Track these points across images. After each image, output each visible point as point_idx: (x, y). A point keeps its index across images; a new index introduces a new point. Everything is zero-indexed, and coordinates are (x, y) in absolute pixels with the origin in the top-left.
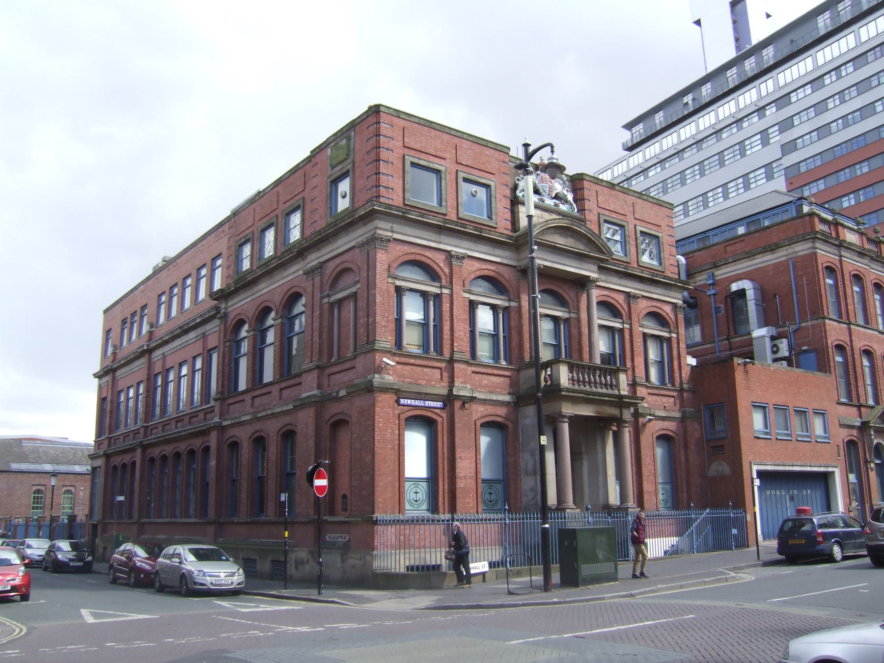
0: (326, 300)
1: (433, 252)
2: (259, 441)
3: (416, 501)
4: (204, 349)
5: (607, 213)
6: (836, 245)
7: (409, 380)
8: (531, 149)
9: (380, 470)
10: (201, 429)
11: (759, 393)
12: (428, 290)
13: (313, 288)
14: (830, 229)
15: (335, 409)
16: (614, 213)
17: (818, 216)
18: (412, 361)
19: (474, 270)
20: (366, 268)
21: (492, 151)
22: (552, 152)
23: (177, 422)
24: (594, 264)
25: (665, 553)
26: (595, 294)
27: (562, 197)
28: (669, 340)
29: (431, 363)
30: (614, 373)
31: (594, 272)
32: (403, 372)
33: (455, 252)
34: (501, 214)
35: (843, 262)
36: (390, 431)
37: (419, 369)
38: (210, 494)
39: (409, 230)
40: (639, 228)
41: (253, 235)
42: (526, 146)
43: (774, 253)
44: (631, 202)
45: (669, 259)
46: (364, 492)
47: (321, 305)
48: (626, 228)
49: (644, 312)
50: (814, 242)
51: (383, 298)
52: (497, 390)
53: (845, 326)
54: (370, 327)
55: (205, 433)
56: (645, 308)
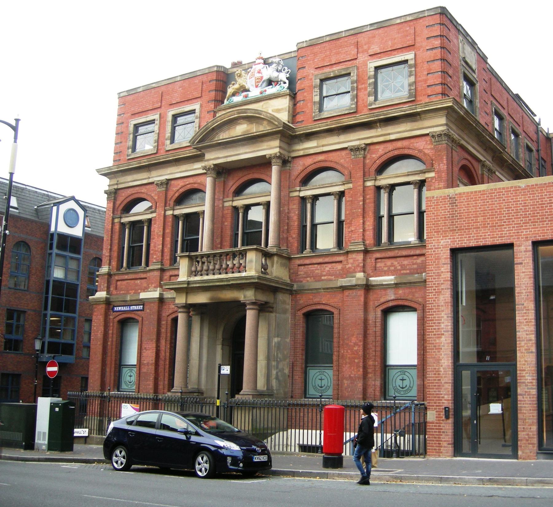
3: (403, 388)
7: (123, 292)
32: (122, 287)
36: (100, 332)
37: (132, 281)
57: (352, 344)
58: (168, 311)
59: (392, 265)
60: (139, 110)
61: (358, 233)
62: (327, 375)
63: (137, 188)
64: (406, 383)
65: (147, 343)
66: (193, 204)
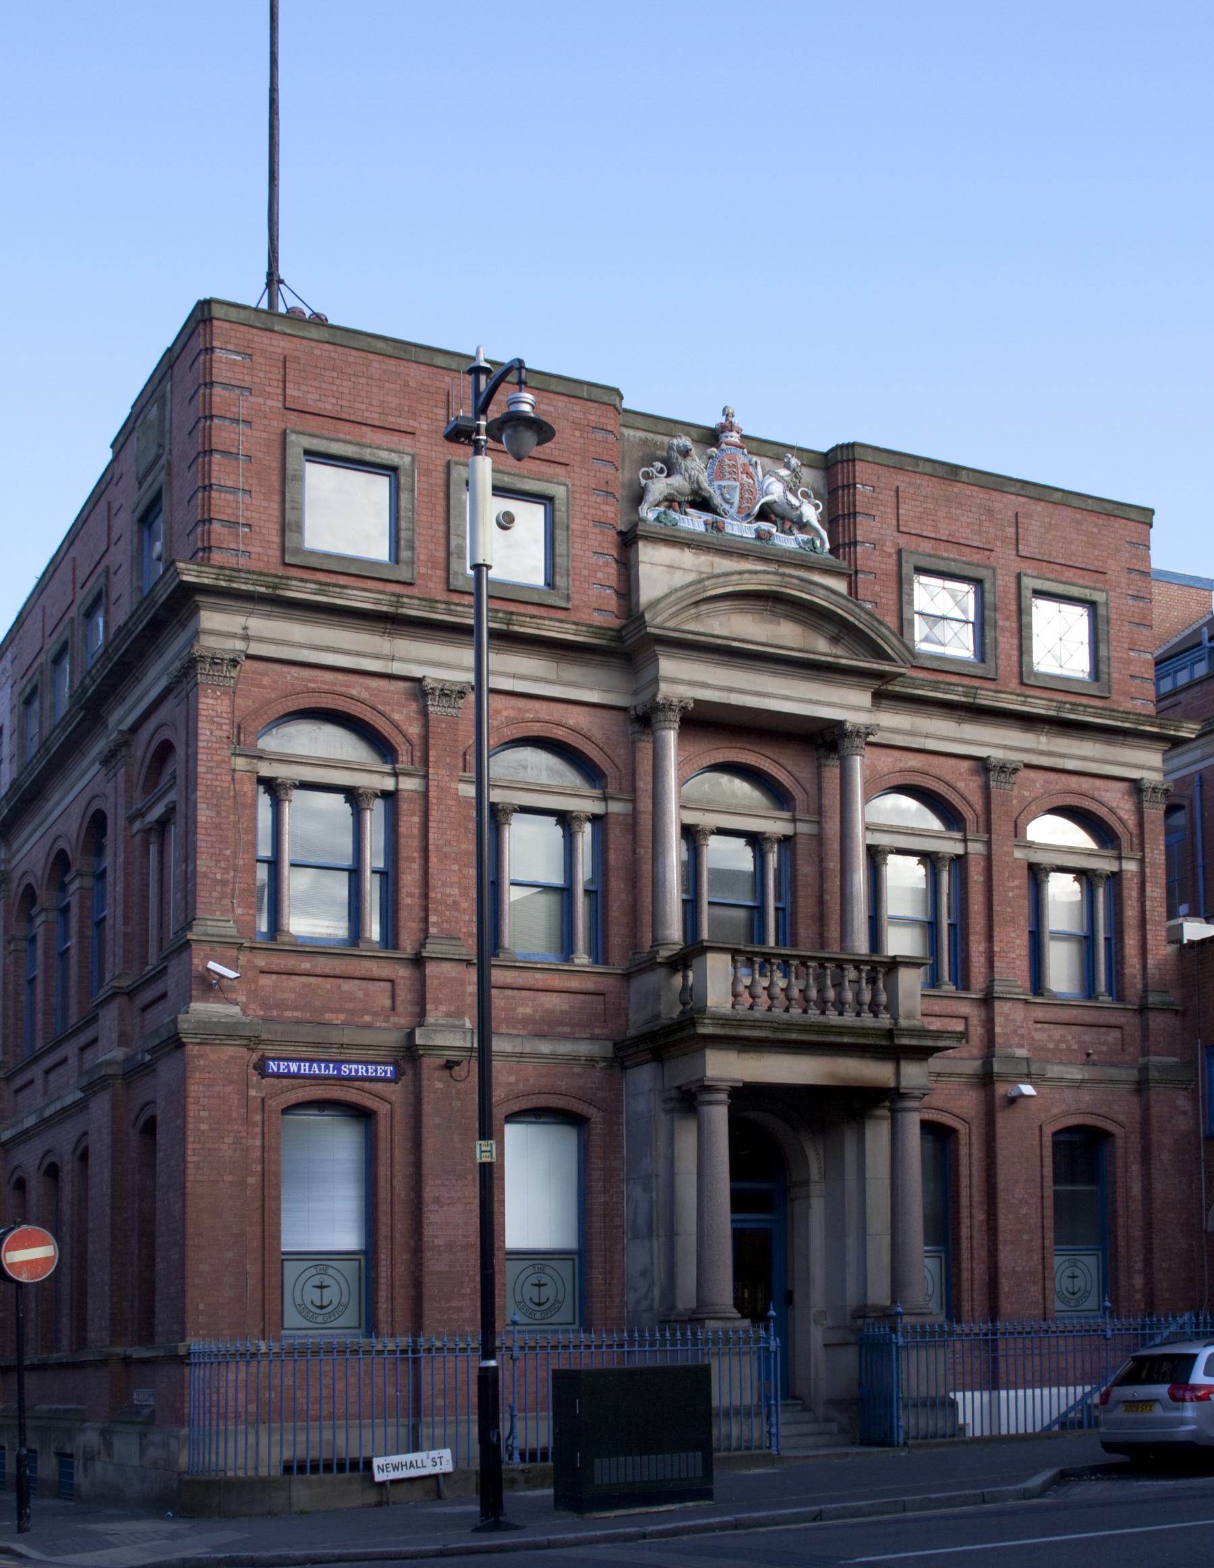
0: (137, 826)
2: (52, 1172)
5: (926, 546)
12: (357, 784)
33: (436, 680)
36: (229, 1140)
37: (328, 984)
41: (42, 673)
52: (560, 1029)
57: (1015, 1201)
60: (320, 404)
61: (1007, 960)
62: (1083, 1267)
63: (329, 676)
65: (443, 1185)
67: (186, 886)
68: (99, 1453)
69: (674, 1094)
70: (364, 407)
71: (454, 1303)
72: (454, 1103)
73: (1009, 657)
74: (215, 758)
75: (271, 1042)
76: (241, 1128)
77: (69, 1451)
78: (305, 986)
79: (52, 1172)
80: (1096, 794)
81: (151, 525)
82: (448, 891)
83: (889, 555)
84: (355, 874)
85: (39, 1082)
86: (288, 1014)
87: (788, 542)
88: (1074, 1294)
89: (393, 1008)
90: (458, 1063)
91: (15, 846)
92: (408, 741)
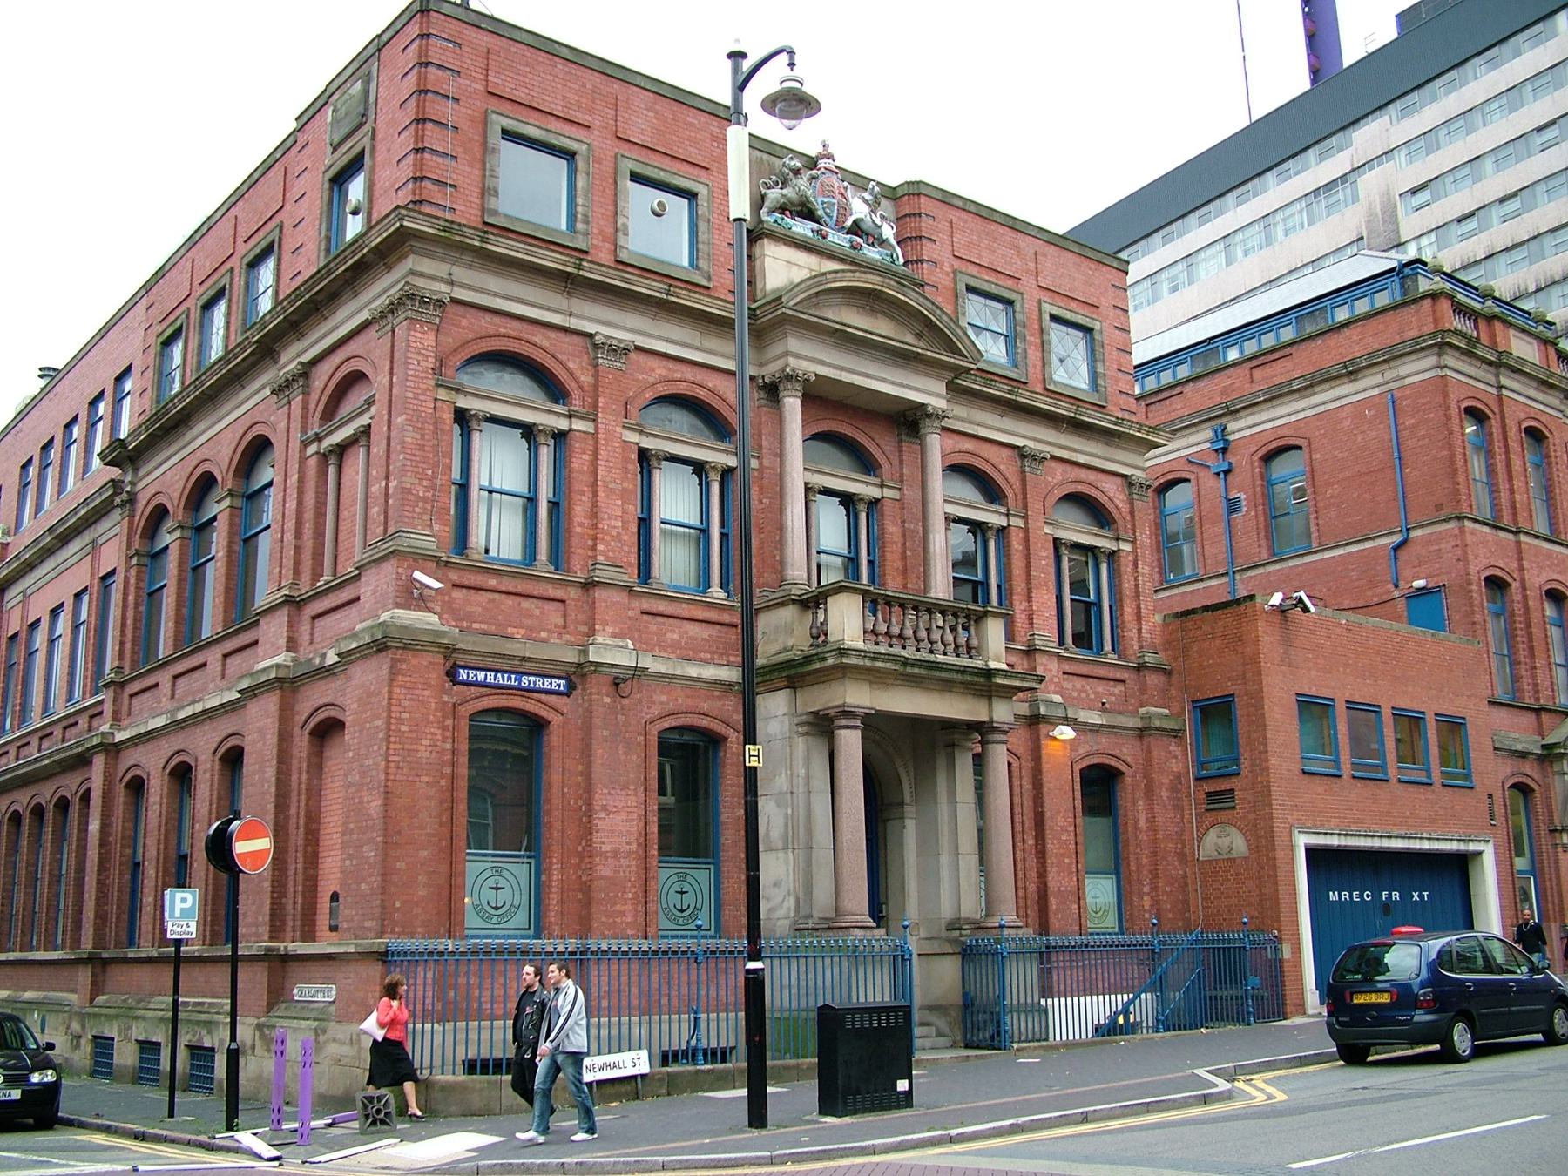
0: (312, 449)
1: (553, 335)
2: (182, 774)
4: (92, 575)
5: (973, 270)
6: (1490, 363)
8: (747, 65)
9: (399, 832)
10: (75, 751)
11: (1313, 673)
12: (538, 422)
13: (289, 423)
14: (1476, 328)
15: (313, 698)
16: (992, 274)
17: (1452, 298)
18: (492, 582)
19: (651, 380)
20: (387, 368)
21: (703, 117)
22: (792, 65)
23: (41, 738)
24: (938, 378)
25: (1097, 1029)
26: (935, 444)
27: (871, 231)
28: (1112, 555)
29: (539, 589)
30: (976, 621)
31: (937, 395)
32: (468, 609)
33: (606, 337)
34: (722, 259)
35: (1504, 399)
36: (426, 742)
37: (510, 601)
38: (86, 896)
39: (493, 282)
40: (1048, 308)
41: (188, 316)
42: (737, 56)
43: (1356, 380)
44: (1032, 251)
45: (1117, 380)
46: (363, 886)
47: (303, 460)
48: (1018, 306)
49: (1058, 494)
50: (1440, 355)
51: (423, 435)
52: (702, 655)
53: (1511, 537)
54: (390, 501)
55: (81, 761)
56: (1060, 484)
58: (649, 708)
59: (1083, 690)
63: (516, 324)
64: (689, 899)
65: (610, 794)
66: (669, 432)
67: (387, 502)
68: (253, 1047)
69: (810, 718)
70: (550, 99)
71: (618, 907)
72: (619, 717)
73: (1035, 366)
74: (421, 386)
75: (464, 651)
76: (437, 731)
77: (207, 1044)
78: (491, 601)
79: (182, 774)
80: (1099, 485)
81: (341, 185)
82: (613, 523)
83: (947, 274)
84: (531, 501)
85: (166, 686)
86: (475, 626)
87: (872, 253)
88: (682, 911)
89: (565, 627)
90: (624, 681)
91: (141, 474)
92: (581, 388)
